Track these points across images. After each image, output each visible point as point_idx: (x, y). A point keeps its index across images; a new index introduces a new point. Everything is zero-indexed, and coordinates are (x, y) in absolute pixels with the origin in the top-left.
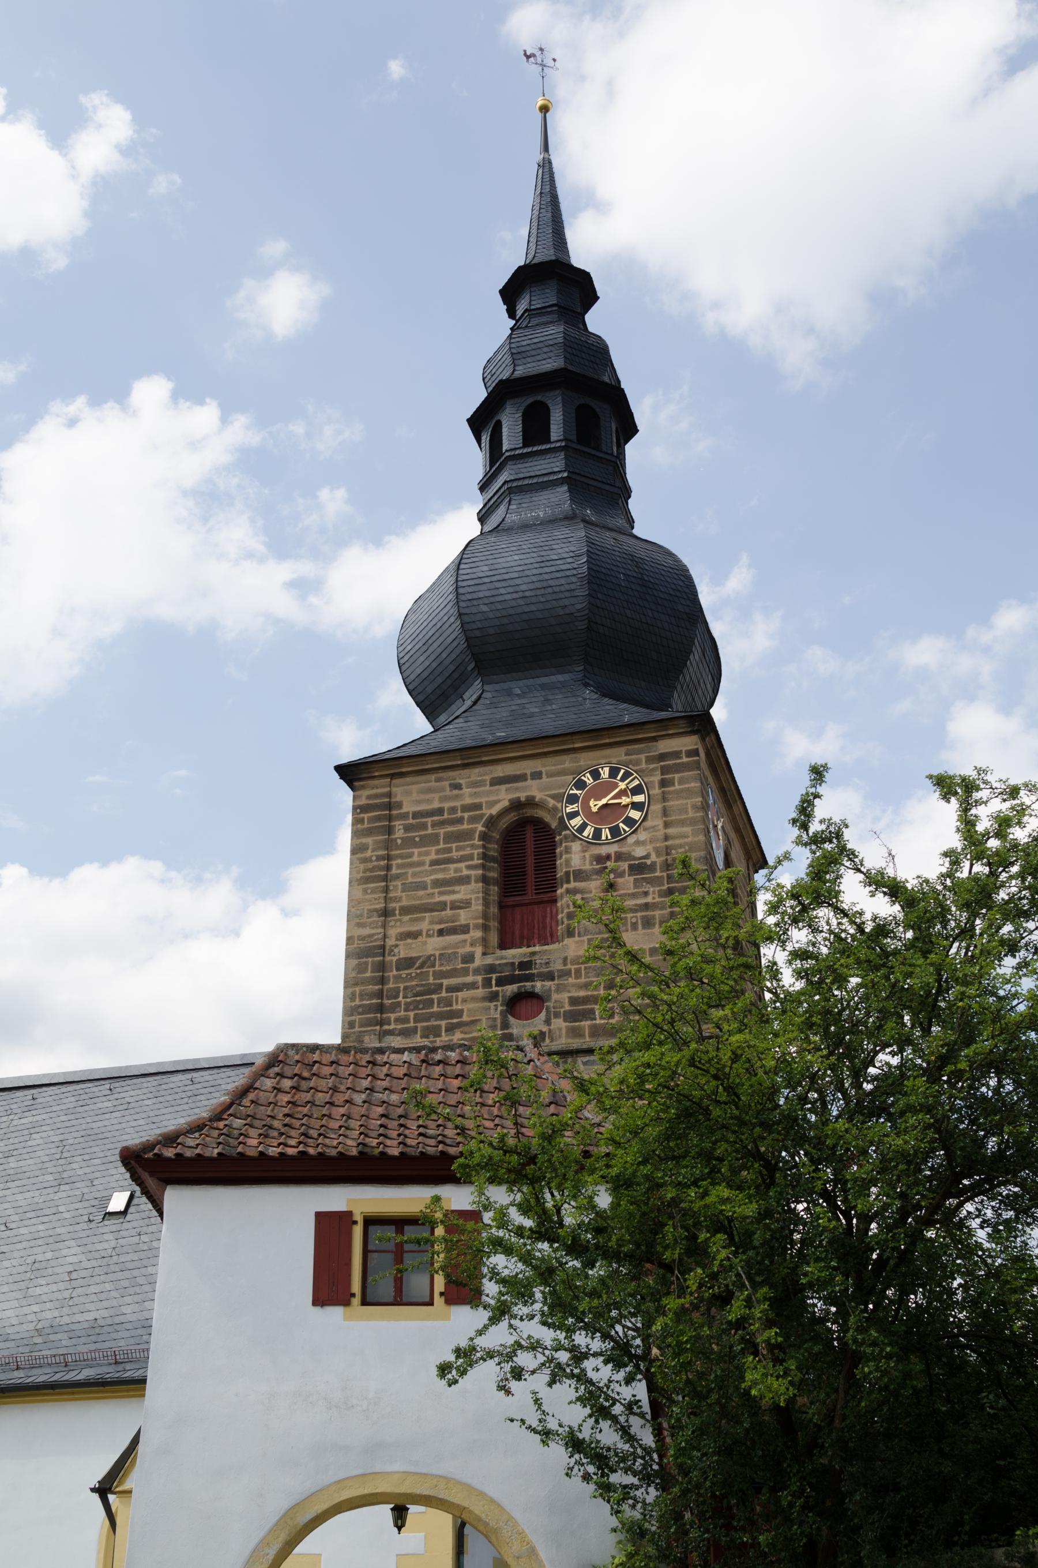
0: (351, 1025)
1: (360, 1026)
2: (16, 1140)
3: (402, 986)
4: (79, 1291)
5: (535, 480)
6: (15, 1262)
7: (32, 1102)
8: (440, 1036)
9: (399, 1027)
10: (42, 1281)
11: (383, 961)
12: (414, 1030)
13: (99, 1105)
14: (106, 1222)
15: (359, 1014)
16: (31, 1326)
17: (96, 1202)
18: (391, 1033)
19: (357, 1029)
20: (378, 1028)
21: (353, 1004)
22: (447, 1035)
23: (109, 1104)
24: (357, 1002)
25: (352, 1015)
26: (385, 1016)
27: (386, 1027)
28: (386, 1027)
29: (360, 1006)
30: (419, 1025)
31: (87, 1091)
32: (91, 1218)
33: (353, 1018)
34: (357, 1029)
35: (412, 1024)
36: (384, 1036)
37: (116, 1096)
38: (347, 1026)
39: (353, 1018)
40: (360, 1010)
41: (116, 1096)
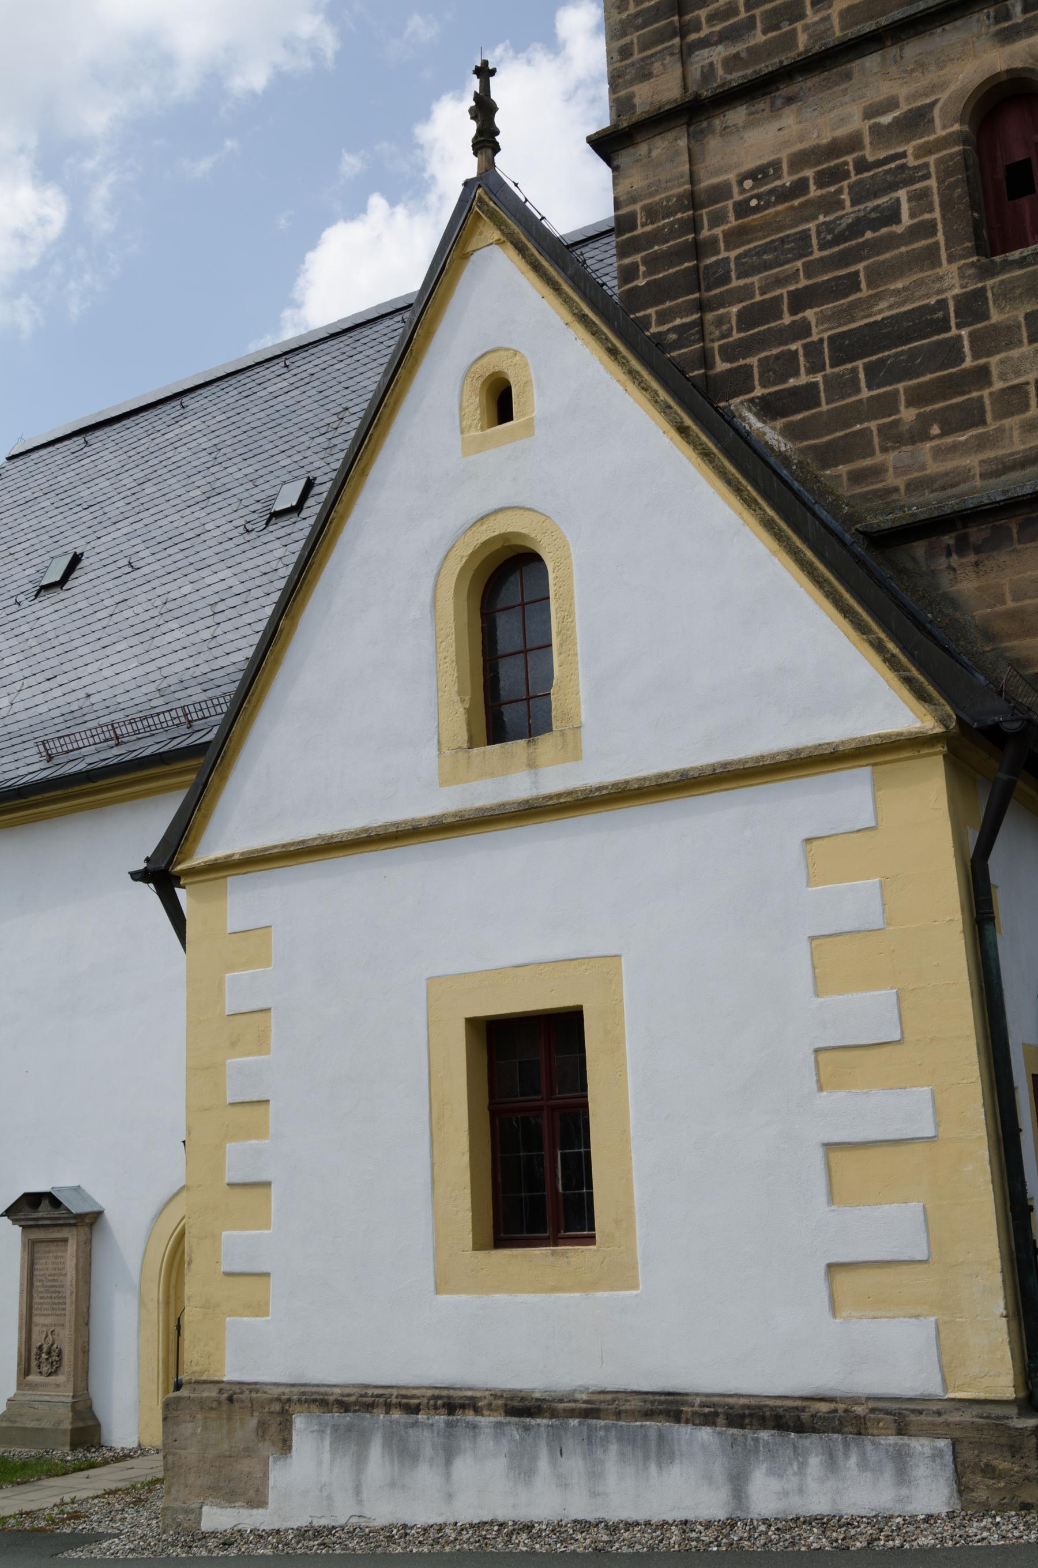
0: (625, 52)
1: (641, 51)
2: (156, 461)
3: (735, 283)
4: (225, 627)
5: (798, 543)
6: (138, 609)
7: (182, 411)
8: (802, 16)
9: (718, 28)
10: (174, 625)
11: (681, 15)
12: (750, 24)
13: (270, 390)
14: (271, 528)
15: (638, 28)
16: (152, 687)
17: (259, 506)
18: (705, 43)
19: (637, 56)
20: (677, 40)
21: (624, 16)
22: (816, 12)
23: (285, 383)
24: (632, 9)
25: (624, 34)
26: (688, 17)
27: (693, 37)
28: (693, 37)
29: (637, 15)
30: (757, 12)
31: (253, 378)
32: (249, 527)
33: (626, 40)
34: (637, 56)
35: (743, 15)
36: (690, 55)
37: (293, 372)
38: (616, 57)
39: (626, 40)
40: (640, 20)
41: (293, 372)
